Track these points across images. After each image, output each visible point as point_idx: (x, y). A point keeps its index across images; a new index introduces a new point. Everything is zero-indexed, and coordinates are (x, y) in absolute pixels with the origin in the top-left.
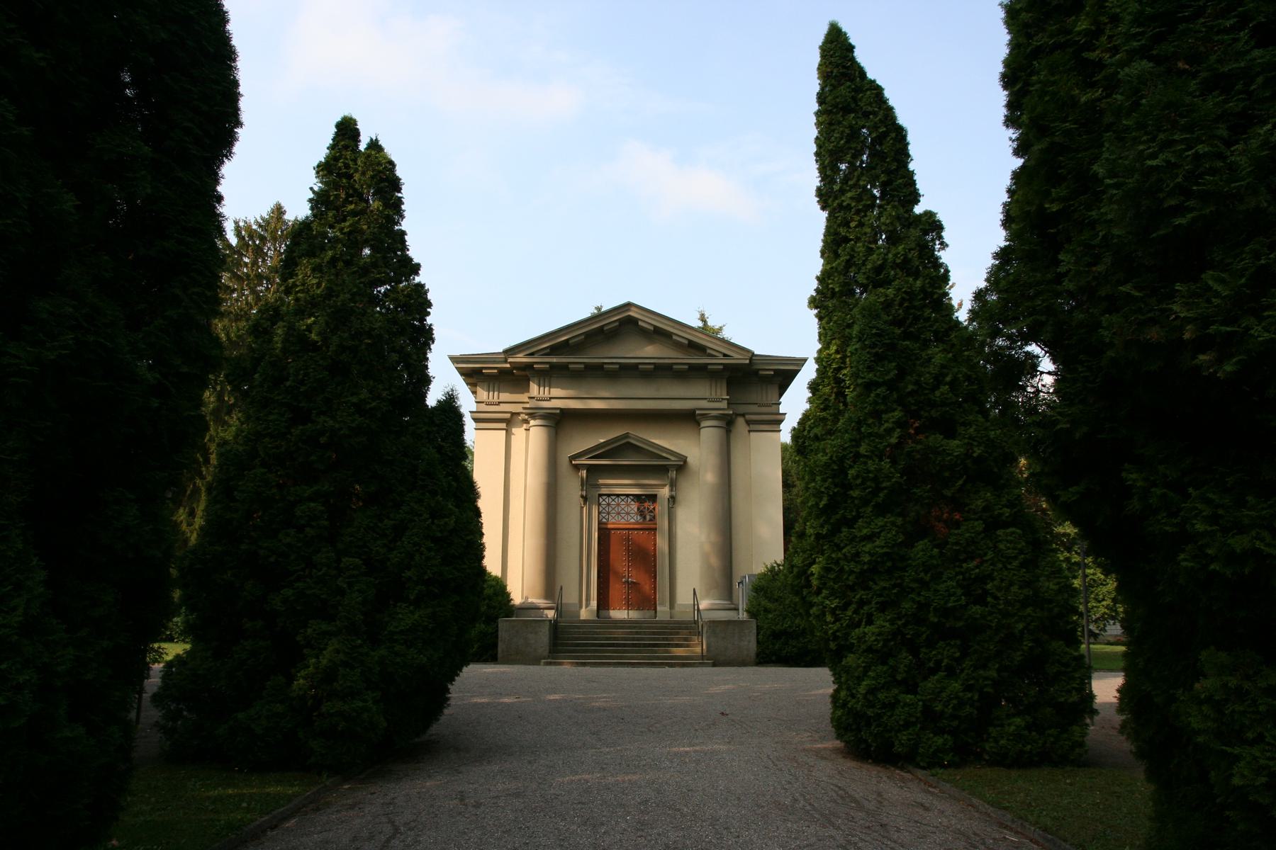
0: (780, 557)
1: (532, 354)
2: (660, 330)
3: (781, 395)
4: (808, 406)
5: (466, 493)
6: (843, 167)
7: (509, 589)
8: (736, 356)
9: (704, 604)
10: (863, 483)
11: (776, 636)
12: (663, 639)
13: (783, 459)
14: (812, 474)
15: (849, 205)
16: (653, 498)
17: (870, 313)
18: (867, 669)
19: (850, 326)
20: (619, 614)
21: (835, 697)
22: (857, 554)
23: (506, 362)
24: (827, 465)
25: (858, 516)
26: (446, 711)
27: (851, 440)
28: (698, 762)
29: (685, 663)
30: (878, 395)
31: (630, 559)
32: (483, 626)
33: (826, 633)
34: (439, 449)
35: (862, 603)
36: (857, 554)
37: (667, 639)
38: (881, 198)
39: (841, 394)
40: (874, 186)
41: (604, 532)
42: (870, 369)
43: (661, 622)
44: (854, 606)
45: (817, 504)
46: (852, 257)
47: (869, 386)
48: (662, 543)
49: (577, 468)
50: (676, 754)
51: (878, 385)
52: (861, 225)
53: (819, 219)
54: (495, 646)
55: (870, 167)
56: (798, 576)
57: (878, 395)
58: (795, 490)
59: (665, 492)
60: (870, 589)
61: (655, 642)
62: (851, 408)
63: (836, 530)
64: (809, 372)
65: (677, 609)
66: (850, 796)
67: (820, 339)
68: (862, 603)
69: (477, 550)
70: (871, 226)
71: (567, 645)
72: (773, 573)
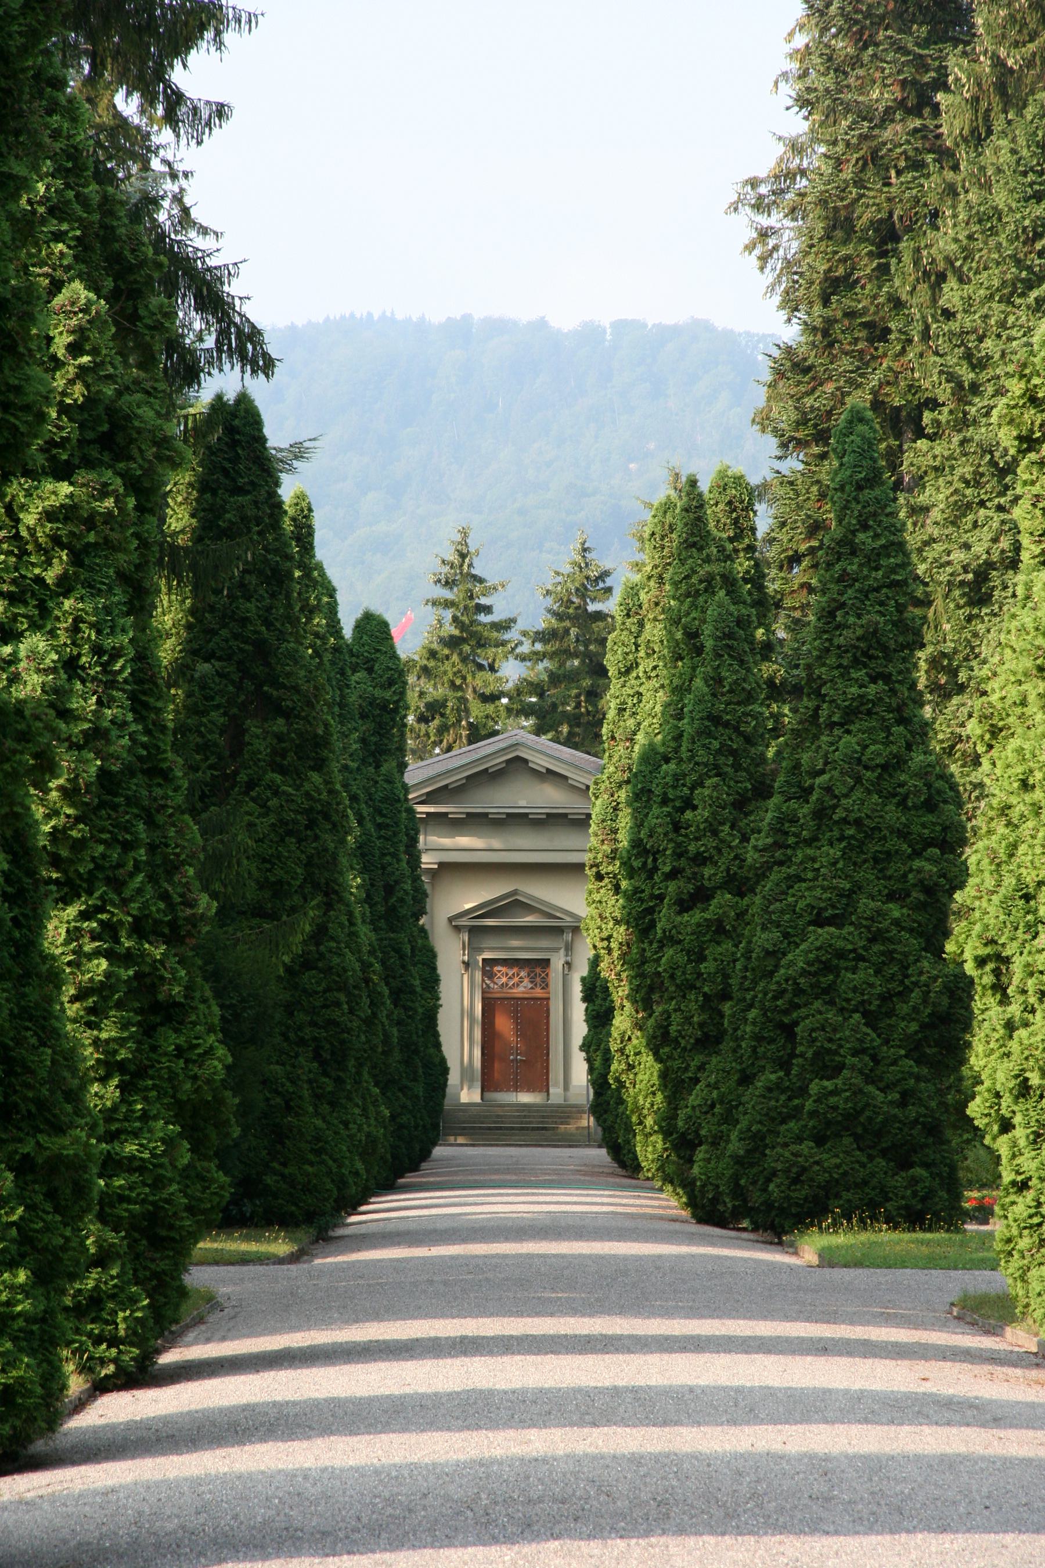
43: (552, 1105)
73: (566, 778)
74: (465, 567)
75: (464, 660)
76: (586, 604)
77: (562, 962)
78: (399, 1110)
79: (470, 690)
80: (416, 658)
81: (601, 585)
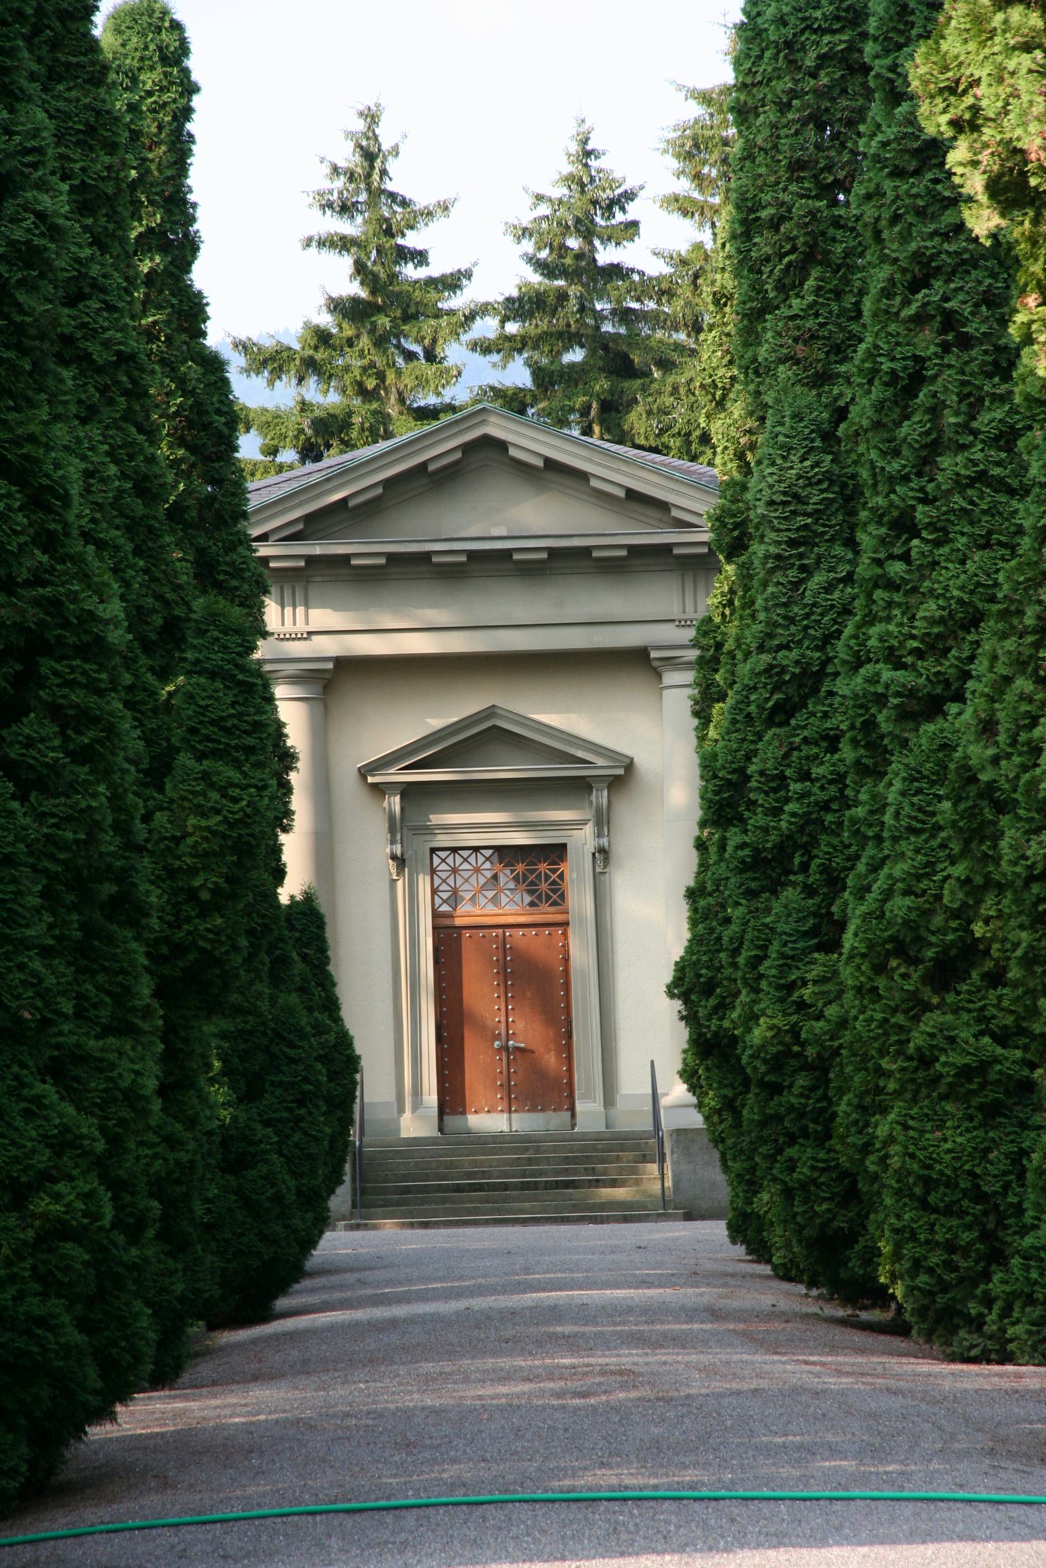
20: (488, 1120)
29: (628, 1214)
37: (593, 1172)
41: (448, 939)
43: (584, 1136)
48: (581, 954)
49: (379, 790)
59: (583, 840)
65: (621, 1104)
73: (583, 476)
74: (376, 177)
75: (380, 342)
76: (593, 249)
77: (590, 846)
78: (43, 1158)
79: (393, 398)
80: (297, 346)
81: (619, 217)
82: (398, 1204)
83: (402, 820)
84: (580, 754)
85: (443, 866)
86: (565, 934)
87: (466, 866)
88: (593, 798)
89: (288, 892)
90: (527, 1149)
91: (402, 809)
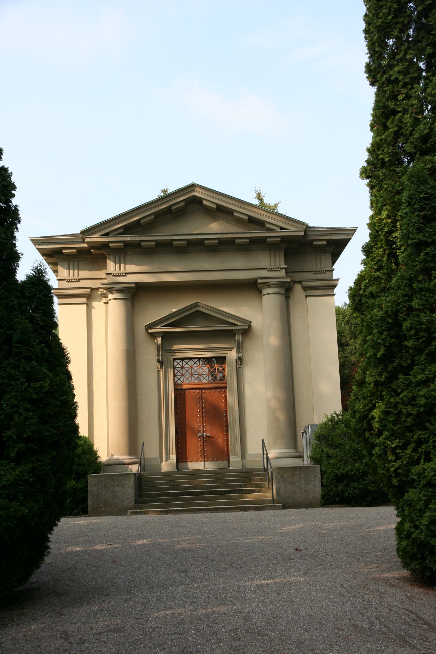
0: (338, 408)
1: (107, 234)
2: (223, 209)
3: (333, 263)
4: (362, 268)
5: (58, 358)
6: (390, 42)
7: (96, 447)
8: (292, 229)
9: (272, 454)
10: (416, 334)
11: (339, 479)
12: (237, 486)
13: (337, 320)
14: (369, 327)
15: (397, 79)
16: (222, 360)
17: (419, 179)
18: (427, 503)
19: (399, 193)
20: (196, 465)
21: (399, 530)
22: (414, 398)
23: (83, 242)
24: (382, 319)
25: (413, 364)
26: (47, 559)
27: (404, 296)
28: (279, 592)
29: (258, 506)
30: (427, 254)
31: (204, 415)
32: (73, 482)
33: (388, 470)
34: (31, 319)
35: (419, 443)
36: (414, 398)
37: (240, 486)
38: (427, 70)
39: (393, 255)
40: (420, 59)
41: (180, 394)
42: (419, 230)
43: (235, 471)
44: (412, 445)
45: (375, 355)
46: (400, 128)
47: (419, 246)
48: (232, 401)
49: (153, 335)
50: (258, 586)
51: (427, 244)
52: (408, 97)
53: (368, 94)
54: (85, 500)
55: (416, 41)
56: (361, 420)
57: (427, 254)
58: (348, 349)
59: (232, 355)
60: (426, 429)
61: (230, 489)
62: (403, 267)
63: (393, 377)
64: (362, 237)
65: (248, 458)
66: (421, 619)
67: (372, 207)
68: (419, 443)
69: (71, 409)
70: (418, 98)
71: (151, 495)
72: (333, 423)
82: (156, 501)
83: (162, 347)
84: (231, 321)
85: (178, 366)
86: (225, 392)
87: (187, 366)
88: (236, 338)
89: (22, 273)
90: (211, 476)
91: (162, 343)
